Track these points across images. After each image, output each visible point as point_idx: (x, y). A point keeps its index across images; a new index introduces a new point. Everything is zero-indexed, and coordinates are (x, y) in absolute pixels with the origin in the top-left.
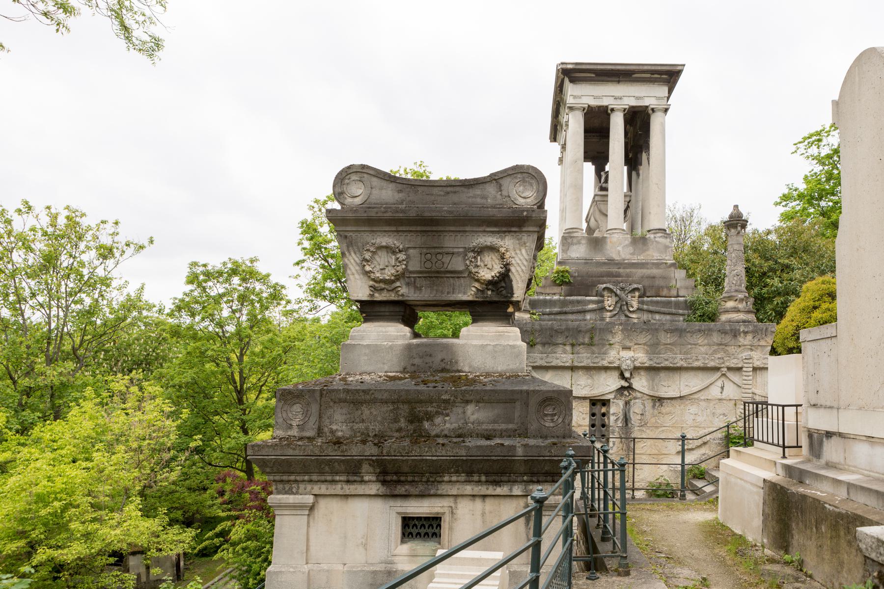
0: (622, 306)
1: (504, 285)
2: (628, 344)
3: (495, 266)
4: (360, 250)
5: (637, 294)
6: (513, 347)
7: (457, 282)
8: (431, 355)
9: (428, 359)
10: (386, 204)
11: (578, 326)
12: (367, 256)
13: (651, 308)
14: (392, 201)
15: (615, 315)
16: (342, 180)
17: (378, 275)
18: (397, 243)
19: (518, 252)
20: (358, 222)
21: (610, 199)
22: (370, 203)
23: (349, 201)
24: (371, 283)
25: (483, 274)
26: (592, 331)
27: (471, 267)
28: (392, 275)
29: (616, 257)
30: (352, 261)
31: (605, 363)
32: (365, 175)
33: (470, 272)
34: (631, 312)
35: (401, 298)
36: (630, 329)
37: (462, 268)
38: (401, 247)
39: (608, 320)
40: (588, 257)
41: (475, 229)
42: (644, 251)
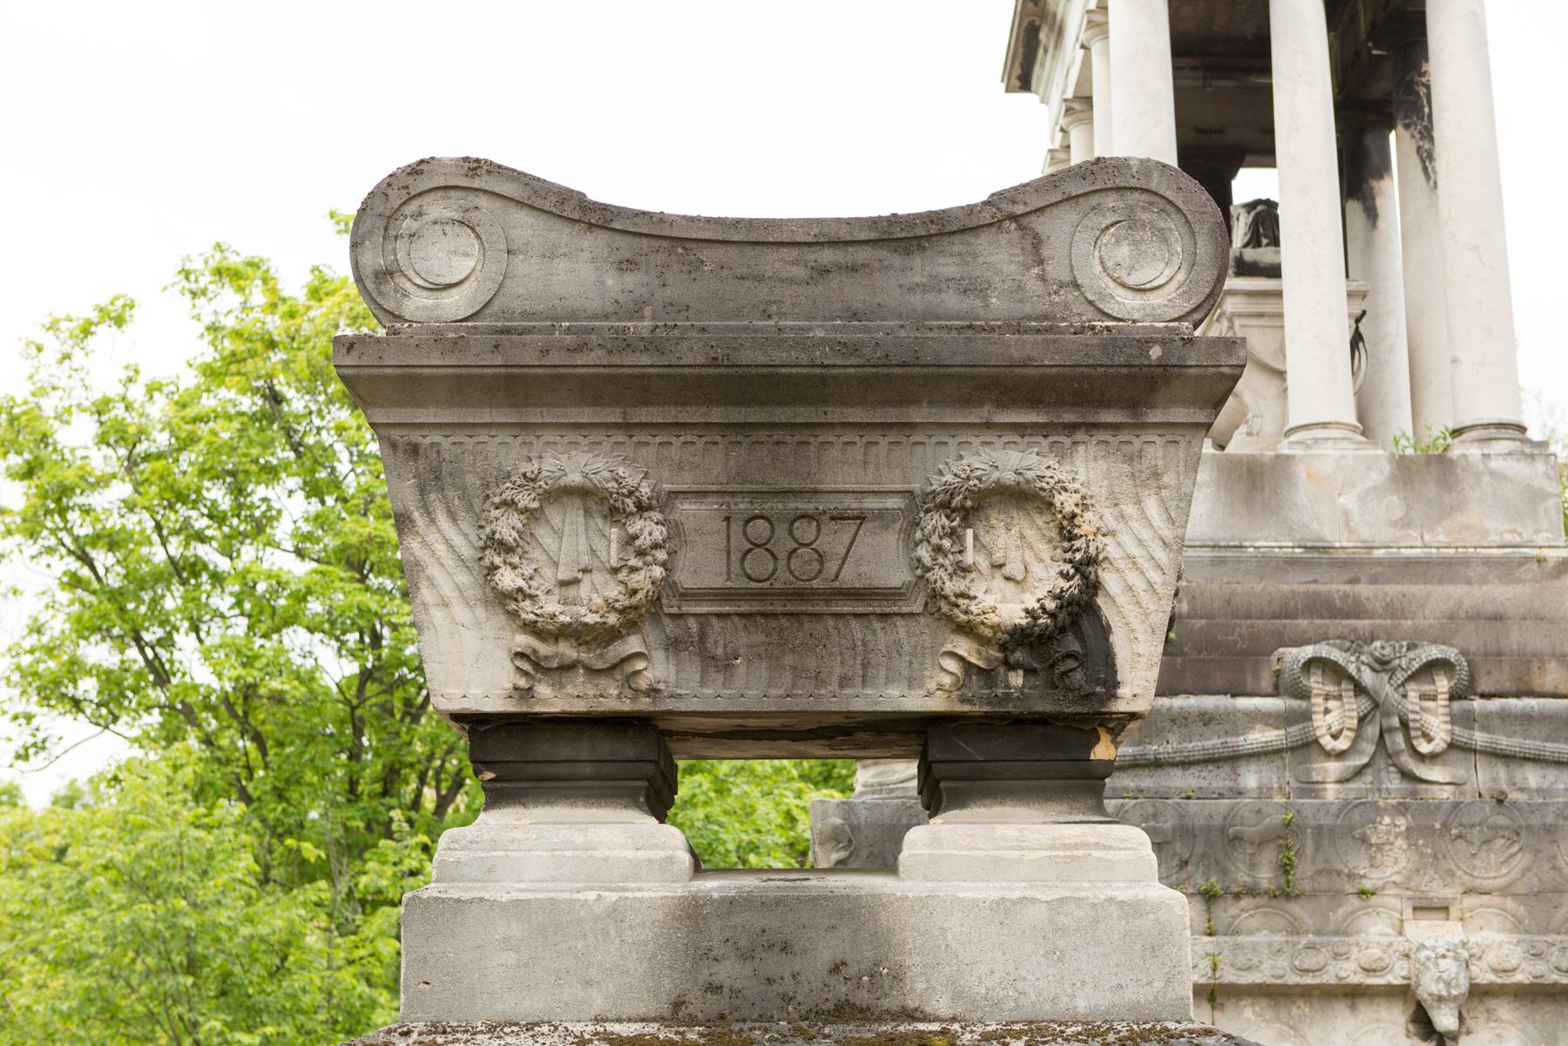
0: (1387, 734)
1: (1075, 647)
2: (1438, 891)
3: (1037, 569)
4: (477, 501)
5: (1443, 684)
6: (1132, 909)
7: (881, 636)
8: (785, 948)
9: (775, 965)
10: (573, 316)
11: (1230, 818)
12: (507, 527)
13: (1505, 742)
14: (594, 305)
15: (1359, 772)
16: (390, 219)
17: (551, 606)
18: (631, 477)
19: (1130, 509)
20: (469, 387)
21: (1290, 305)
22: (504, 314)
23: (418, 304)
24: (523, 641)
25: (988, 601)
26: (1285, 836)
27: (938, 574)
28: (610, 606)
29: (1338, 538)
30: (441, 549)
31: (1350, 972)
32: (483, 201)
33: (936, 595)
34: (1422, 757)
35: (645, 704)
36: (1440, 829)
37: (897, 576)
38: (645, 490)
39: (1331, 793)
40: (1223, 537)
41: (949, 416)
42: (1449, 511)
